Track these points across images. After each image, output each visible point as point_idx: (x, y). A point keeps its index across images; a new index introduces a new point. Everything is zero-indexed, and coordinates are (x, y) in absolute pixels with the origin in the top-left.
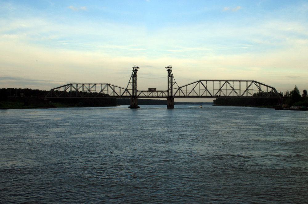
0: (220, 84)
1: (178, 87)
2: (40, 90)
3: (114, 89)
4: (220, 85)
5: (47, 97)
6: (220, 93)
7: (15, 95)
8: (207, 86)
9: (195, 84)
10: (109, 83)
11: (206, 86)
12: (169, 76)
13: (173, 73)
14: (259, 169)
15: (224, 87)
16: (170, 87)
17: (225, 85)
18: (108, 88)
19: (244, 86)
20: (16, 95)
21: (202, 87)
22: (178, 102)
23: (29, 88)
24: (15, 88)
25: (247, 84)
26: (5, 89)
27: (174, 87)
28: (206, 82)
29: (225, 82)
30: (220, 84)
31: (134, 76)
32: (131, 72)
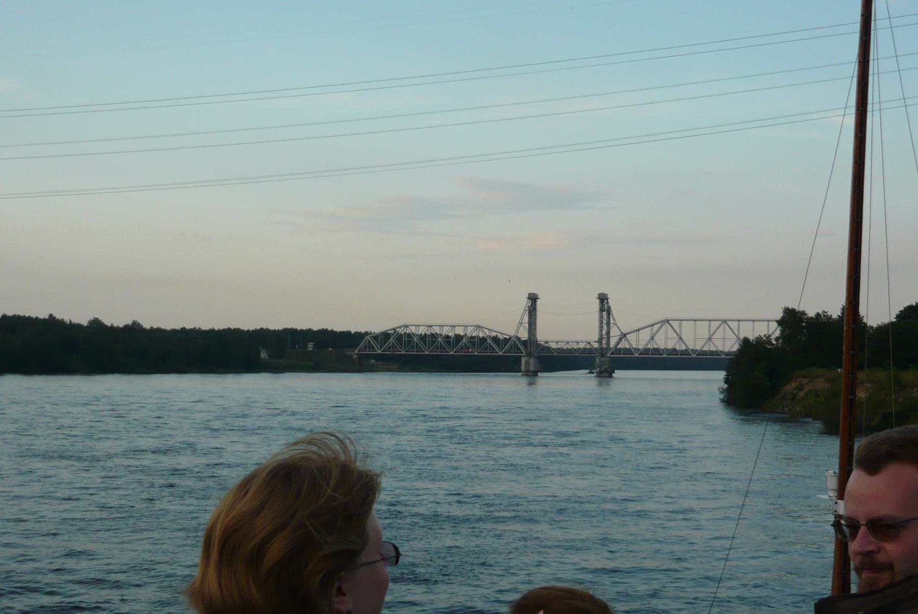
0: (710, 326)
1: (620, 334)
2: (251, 330)
3: (681, 332)
4: (710, 330)
5: (359, 351)
6: (709, 346)
7: (297, 346)
8: (739, 332)
9: (656, 327)
10: (669, 317)
11: (737, 334)
12: (602, 310)
13: (611, 302)
14: (337, 447)
15: (719, 334)
16: (604, 332)
17: (661, 331)
18: (666, 332)
19: (703, 330)
20: (299, 347)
21: (672, 334)
22: (184, 335)
23: (265, 328)
24: (299, 329)
25: (652, 330)
26: (326, 330)
27: (612, 334)
28: (767, 322)
29: (719, 323)
30: (710, 326)
31: (532, 311)
32: (524, 303)
